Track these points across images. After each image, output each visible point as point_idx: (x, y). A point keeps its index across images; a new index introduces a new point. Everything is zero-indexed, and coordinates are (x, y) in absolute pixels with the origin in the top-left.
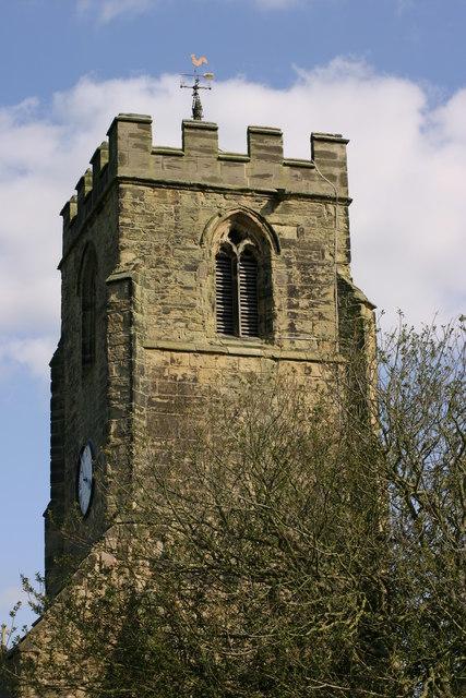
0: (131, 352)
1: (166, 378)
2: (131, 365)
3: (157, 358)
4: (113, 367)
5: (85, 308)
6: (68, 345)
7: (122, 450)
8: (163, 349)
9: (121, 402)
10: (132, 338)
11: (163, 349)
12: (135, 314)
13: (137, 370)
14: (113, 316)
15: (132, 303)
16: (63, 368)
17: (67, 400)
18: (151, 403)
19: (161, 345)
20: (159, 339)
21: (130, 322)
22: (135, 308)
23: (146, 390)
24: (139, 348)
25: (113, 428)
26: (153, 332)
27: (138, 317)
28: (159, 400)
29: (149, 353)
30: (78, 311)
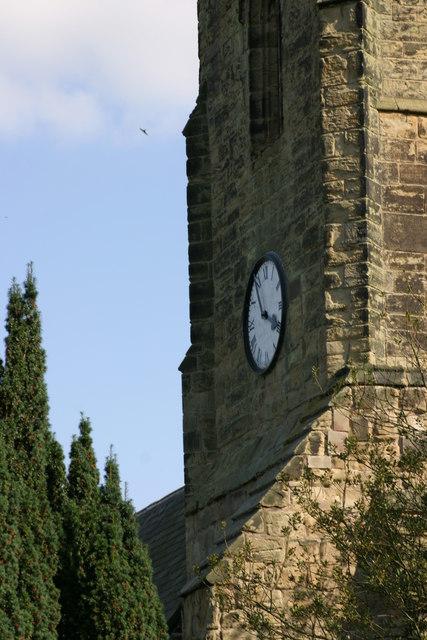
0: (361, 118)
1: (411, 158)
2: (362, 138)
3: (397, 126)
4: (332, 141)
5: (253, 42)
6: (218, 101)
7: (350, 272)
8: (407, 112)
9: (345, 196)
10: (362, 95)
11: (407, 112)
12: (366, 56)
13: (370, 148)
14: (330, 58)
15: (361, 38)
16: (206, 139)
17: (216, 187)
18: (390, 198)
19: (404, 105)
20: (399, 95)
21: (358, 69)
22: (366, 46)
23: (382, 178)
24: (372, 112)
25: (334, 236)
26: (389, 86)
27: (370, 60)
28: (401, 193)
29: (386, 118)
30: (239, 49)
